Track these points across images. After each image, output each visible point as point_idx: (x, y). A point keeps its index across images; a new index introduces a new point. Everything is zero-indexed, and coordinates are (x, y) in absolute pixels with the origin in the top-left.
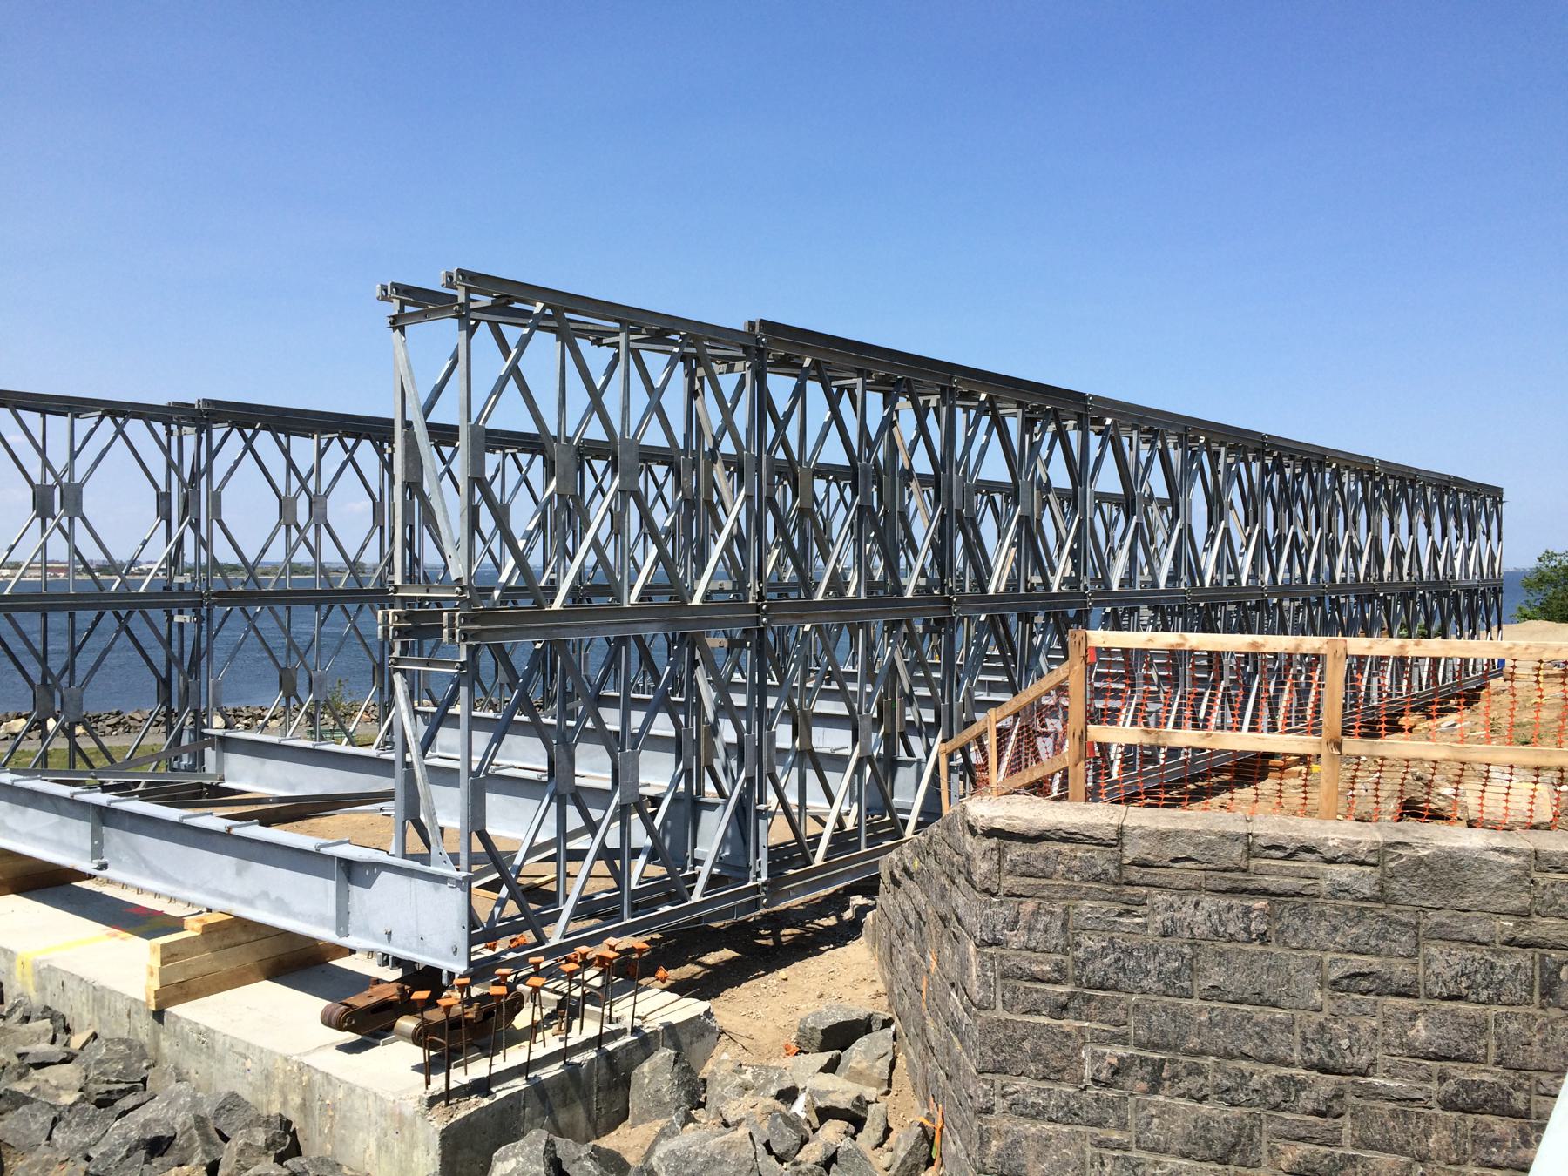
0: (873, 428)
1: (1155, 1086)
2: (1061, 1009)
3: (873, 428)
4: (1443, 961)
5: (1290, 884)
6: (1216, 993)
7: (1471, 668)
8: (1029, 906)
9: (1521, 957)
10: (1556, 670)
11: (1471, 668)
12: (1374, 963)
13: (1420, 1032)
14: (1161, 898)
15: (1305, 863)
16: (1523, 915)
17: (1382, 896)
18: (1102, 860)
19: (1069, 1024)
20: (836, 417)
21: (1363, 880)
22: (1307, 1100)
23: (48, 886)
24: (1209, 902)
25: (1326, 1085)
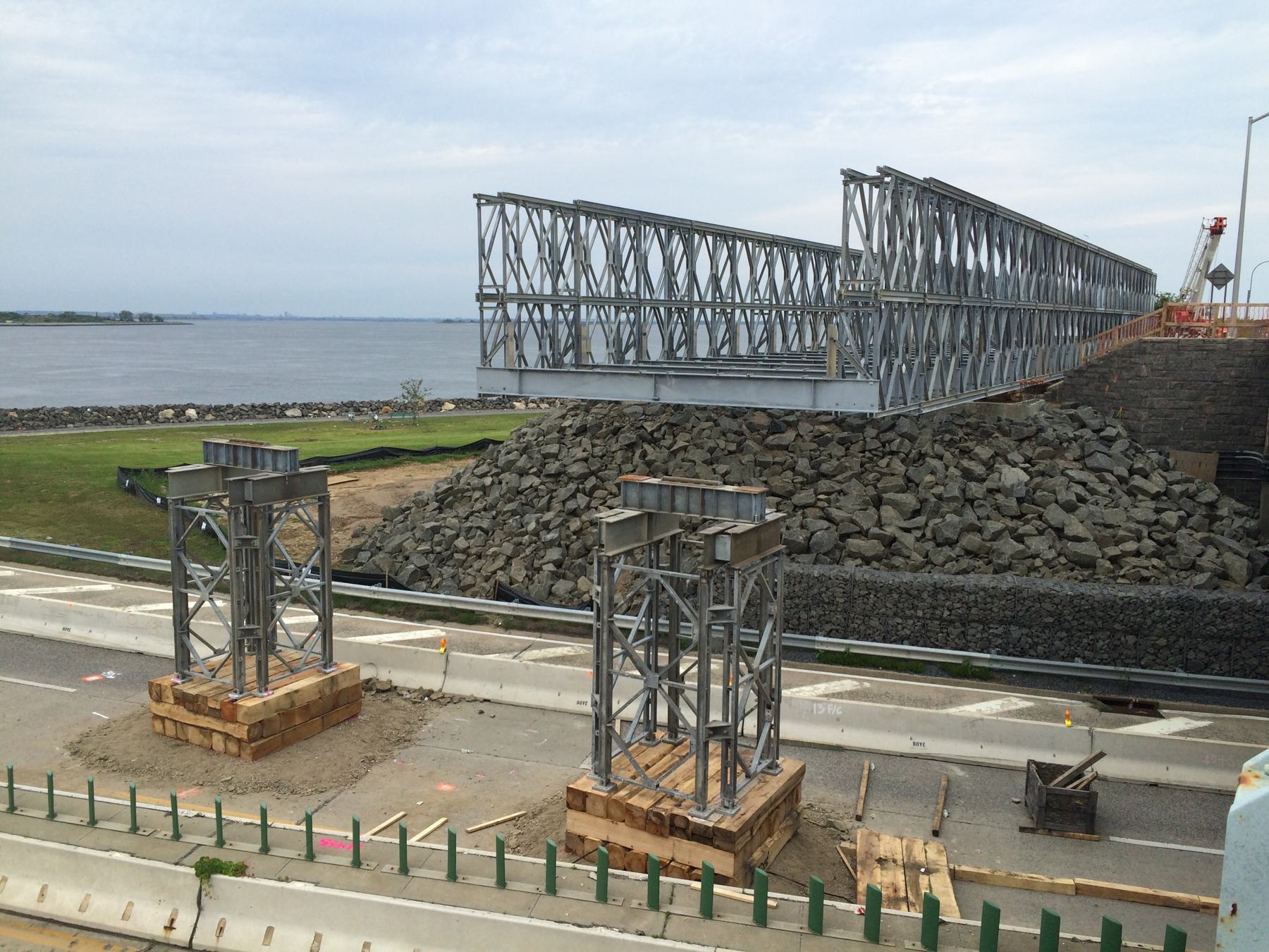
0: (547, 226)
1: (1182, 387)
2: (1164, 375)
3: (547, 226)
4: (1238, 360)
5: (1211, 348)
6: (1196, 369)
7: (1062, 366)
8: (1159, 356)
9: (1251, 359)
10: (251, 663)
11: (1062, 366)
12: (1226, 362)
13: (1233, 373)
14: (1186, 352)
15: (1215, 344)
16: (1252, 351)
17: (1228, 349)
18: (1175, 347)
19: (1165, 378)
20: (531, 220)
21: (1224, 346)
22: (1211, 387)
23: (26, 563)
24: (1195, 353)
25: (1215, 385)
